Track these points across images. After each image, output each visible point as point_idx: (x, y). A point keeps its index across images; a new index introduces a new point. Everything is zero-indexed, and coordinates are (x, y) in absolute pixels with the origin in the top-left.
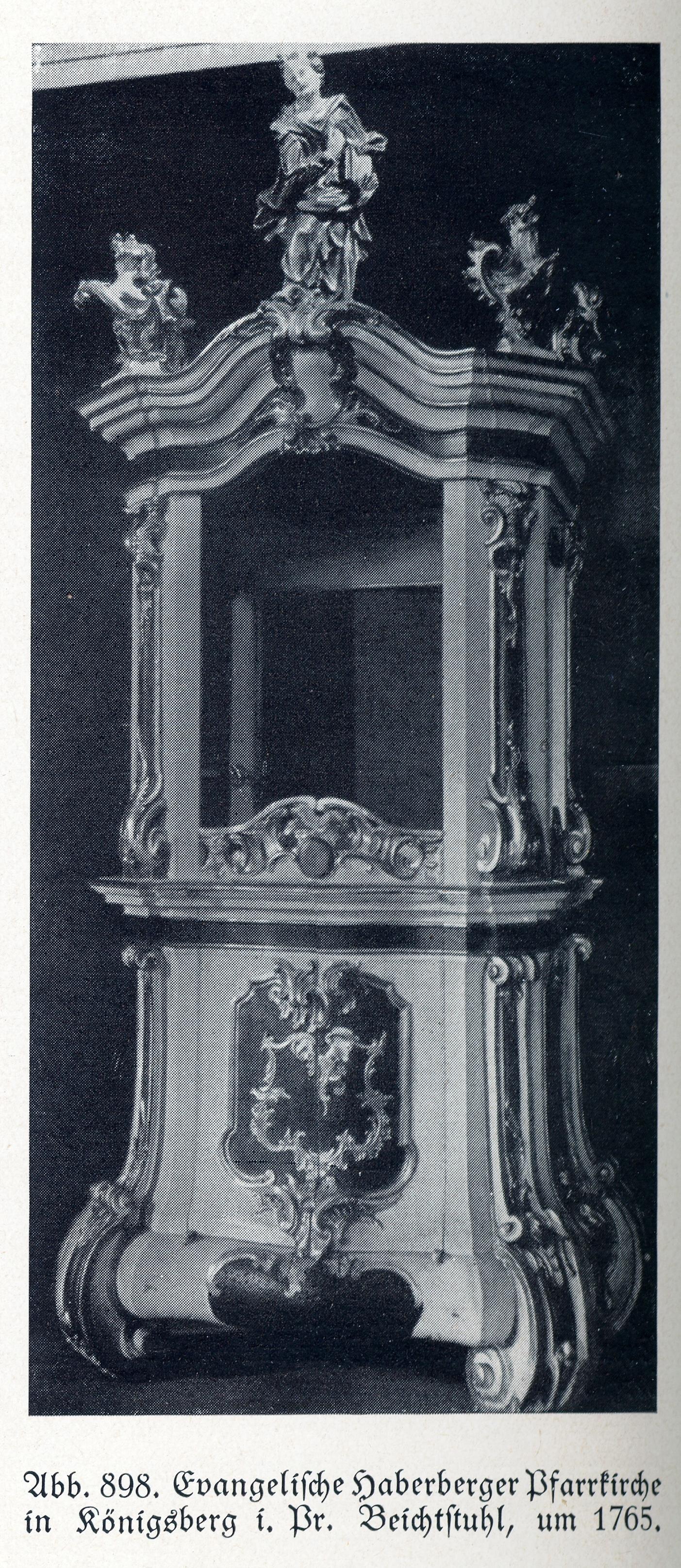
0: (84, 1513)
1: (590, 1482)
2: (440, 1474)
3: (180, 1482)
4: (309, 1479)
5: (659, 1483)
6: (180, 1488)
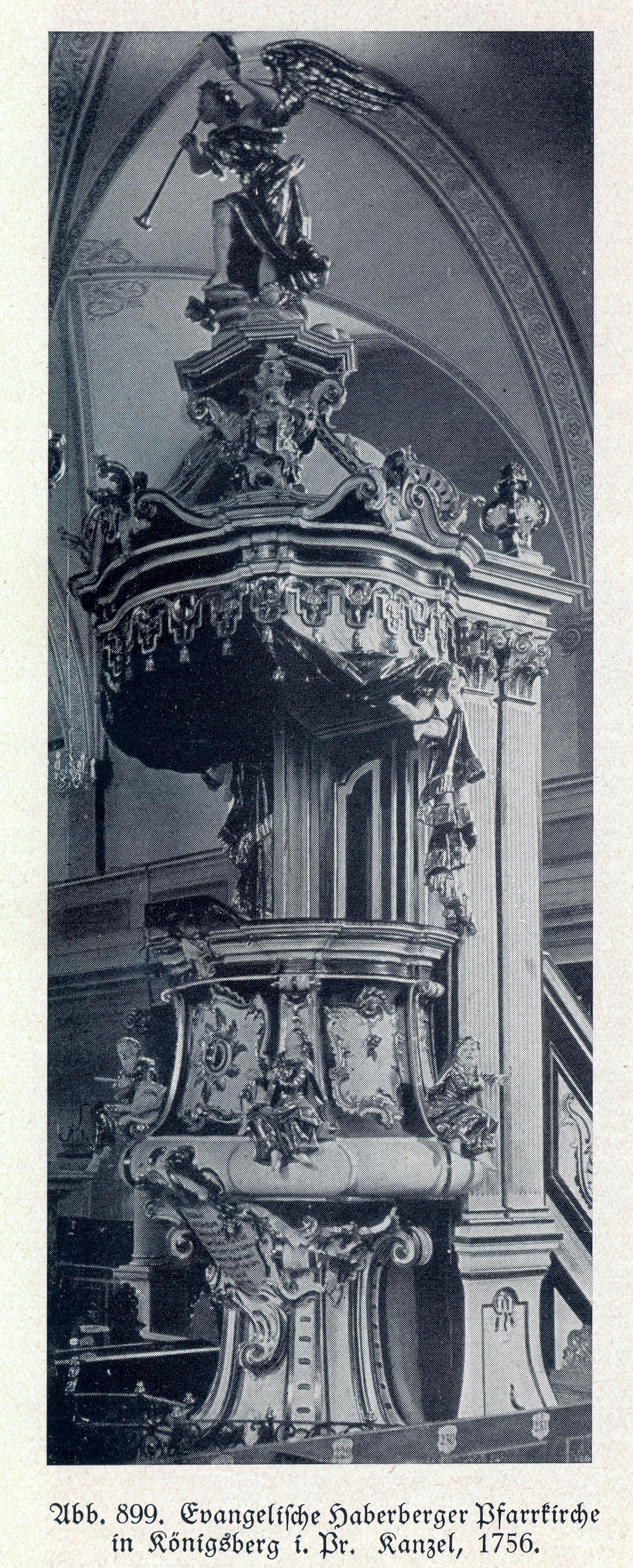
0: (154, 1536)
1: (533, 1512)
2: (401, 1507)
3: (186, 1511)
4: (291, 1511)
5: (318, 1514)
6: (186, 1516)
